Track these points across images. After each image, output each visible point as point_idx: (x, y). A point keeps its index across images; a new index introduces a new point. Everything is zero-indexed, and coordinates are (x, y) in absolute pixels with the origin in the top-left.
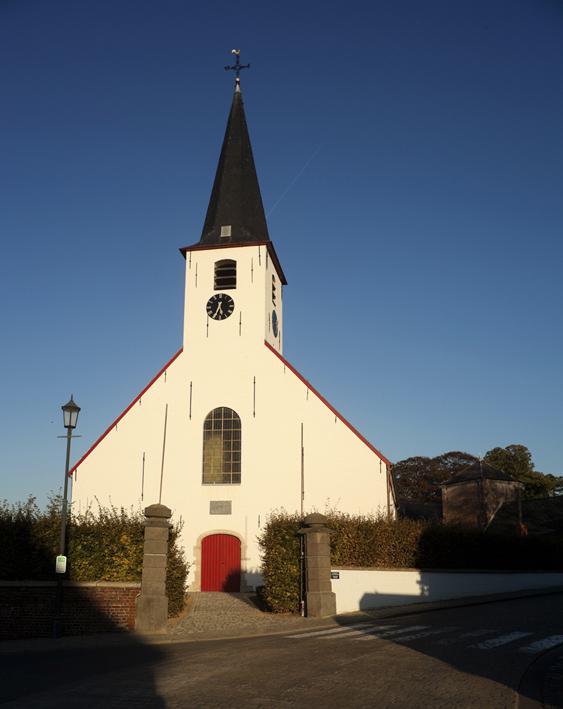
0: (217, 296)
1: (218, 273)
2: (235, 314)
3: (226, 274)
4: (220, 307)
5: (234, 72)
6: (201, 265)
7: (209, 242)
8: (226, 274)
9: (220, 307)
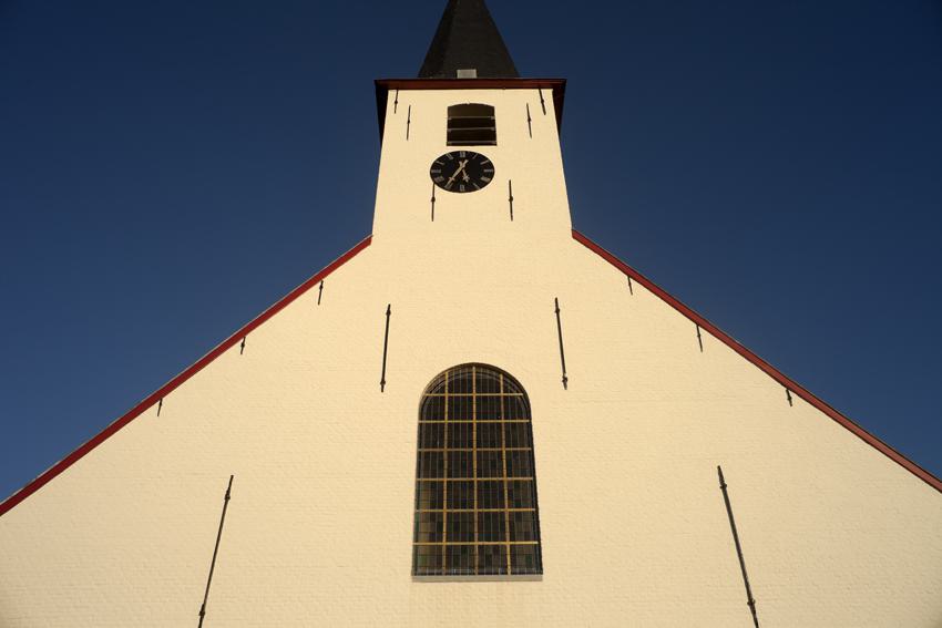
1: (451, 124)
3: (472, 126)
4: (462, 171)
7: (433, 76)
8: (472, 126)
9: (462, 171)
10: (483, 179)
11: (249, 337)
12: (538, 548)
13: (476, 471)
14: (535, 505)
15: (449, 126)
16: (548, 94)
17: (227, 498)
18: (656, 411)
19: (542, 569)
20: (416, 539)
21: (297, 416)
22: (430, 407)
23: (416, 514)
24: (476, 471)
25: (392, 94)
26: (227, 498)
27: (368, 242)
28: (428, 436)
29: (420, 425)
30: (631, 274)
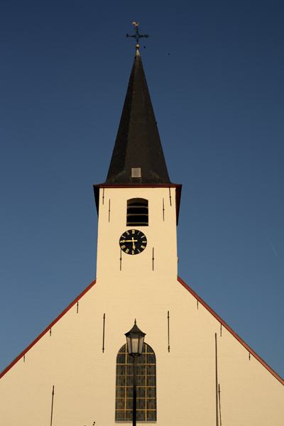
0: (130, 231)
1: (129, 211)
2: (148, 250)
3: (138, 212)
4: (133, 243)
5: (134, 39)
6: (115, 201)
7: (118, 179)
8: (138, 212)
9: (133, 243)
10: (142, 247)
11: (53, 328)
12: (156, 412)
13: (136, 373)
14: (156, 397)
15: (128, 205)
16: (173, 190)
17: (53, 394)
18: (195, 348)
19: (156, 418)
20: (117, 385)
21: (76, 354)
22: (120, 358)
23: (116, 400)
24: (136, 373)
25: (101, 190)
26: (53, 394)
27: (94, 283)
28: (120, 370)
29: (117, 366)
30: (252, 351)
